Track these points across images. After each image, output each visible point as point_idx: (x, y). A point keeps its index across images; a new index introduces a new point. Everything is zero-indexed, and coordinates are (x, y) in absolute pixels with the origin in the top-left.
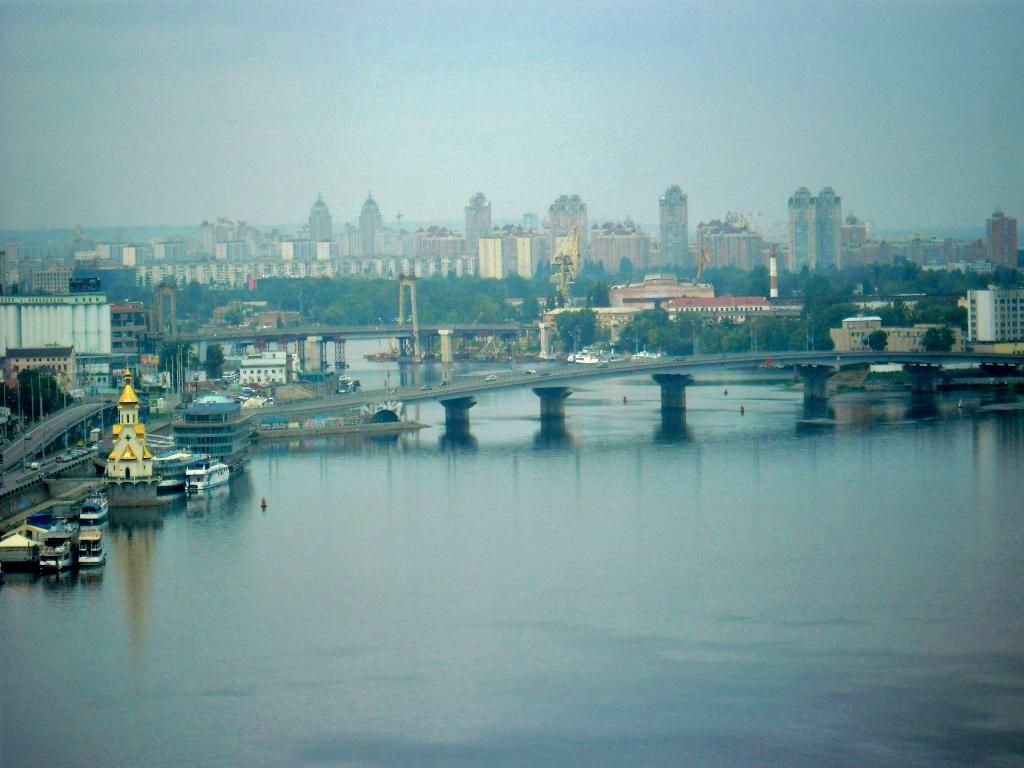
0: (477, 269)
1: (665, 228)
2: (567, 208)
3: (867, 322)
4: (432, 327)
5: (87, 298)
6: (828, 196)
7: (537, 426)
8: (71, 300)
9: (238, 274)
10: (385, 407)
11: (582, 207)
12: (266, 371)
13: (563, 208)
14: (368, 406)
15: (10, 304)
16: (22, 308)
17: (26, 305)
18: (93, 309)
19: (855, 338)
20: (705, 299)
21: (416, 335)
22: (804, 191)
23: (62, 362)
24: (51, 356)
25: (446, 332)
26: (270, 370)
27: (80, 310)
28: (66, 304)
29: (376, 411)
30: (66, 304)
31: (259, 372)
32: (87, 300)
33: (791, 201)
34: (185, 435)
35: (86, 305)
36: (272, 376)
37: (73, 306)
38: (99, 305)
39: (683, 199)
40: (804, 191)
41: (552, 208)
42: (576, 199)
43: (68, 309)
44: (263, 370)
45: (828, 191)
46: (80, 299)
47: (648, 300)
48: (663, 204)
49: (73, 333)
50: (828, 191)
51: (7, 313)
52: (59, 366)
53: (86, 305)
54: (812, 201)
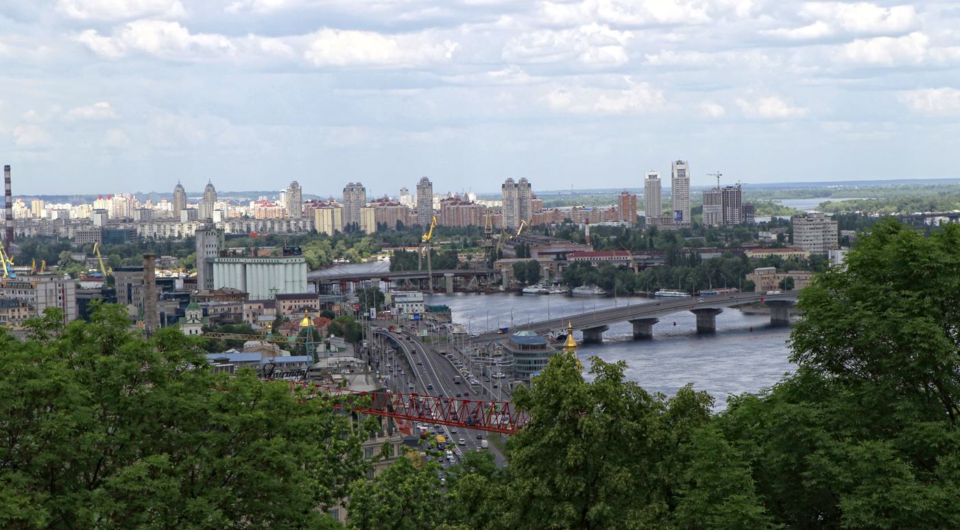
0: (313, 226)
1: (420, 202)
2: (354, 190)
3: (769, 270)
4: (440, 272)
5: (294, 259)
6: (524, 183)
7: (275, 318)
8: (284, 261)
9: (172, 230)
10: (562, 334)
11: (363, 189)
12: (412, 305)
13: (352, 190)
14: (553, 332)
15: (237, 263)
16: (248, 266)
17: (251, 264)
18: (297, 266)
19: (764, 281)
20: (588, 253)
21: (431, 277)
22: (510, 180)
24: (297, 299)
25: (450, 275)
26: (414, 304)
27: (290, 266)
28: (281, 263)
29: (557, 336)
30: (281, 263)
31: (408, 306)
32: (294, 261)
33: (503, 186)
34: (519, 358)
35: (293, 264)
36: (416, 308)
37: (286, 264)
38: (300, 264)
39: (430, 185)
40: (510, 180)
41: (344, 190)
42: (359, 185)
43: (282, 267)
44: (410, 304)
45: (523, 180)
46: (290, 260)
47: (553, 253)
48: (419, 187)
49: (286, 282)
50: (523, 180)
51: (251, 267)
53: (293, 264)
54: (516, 185)
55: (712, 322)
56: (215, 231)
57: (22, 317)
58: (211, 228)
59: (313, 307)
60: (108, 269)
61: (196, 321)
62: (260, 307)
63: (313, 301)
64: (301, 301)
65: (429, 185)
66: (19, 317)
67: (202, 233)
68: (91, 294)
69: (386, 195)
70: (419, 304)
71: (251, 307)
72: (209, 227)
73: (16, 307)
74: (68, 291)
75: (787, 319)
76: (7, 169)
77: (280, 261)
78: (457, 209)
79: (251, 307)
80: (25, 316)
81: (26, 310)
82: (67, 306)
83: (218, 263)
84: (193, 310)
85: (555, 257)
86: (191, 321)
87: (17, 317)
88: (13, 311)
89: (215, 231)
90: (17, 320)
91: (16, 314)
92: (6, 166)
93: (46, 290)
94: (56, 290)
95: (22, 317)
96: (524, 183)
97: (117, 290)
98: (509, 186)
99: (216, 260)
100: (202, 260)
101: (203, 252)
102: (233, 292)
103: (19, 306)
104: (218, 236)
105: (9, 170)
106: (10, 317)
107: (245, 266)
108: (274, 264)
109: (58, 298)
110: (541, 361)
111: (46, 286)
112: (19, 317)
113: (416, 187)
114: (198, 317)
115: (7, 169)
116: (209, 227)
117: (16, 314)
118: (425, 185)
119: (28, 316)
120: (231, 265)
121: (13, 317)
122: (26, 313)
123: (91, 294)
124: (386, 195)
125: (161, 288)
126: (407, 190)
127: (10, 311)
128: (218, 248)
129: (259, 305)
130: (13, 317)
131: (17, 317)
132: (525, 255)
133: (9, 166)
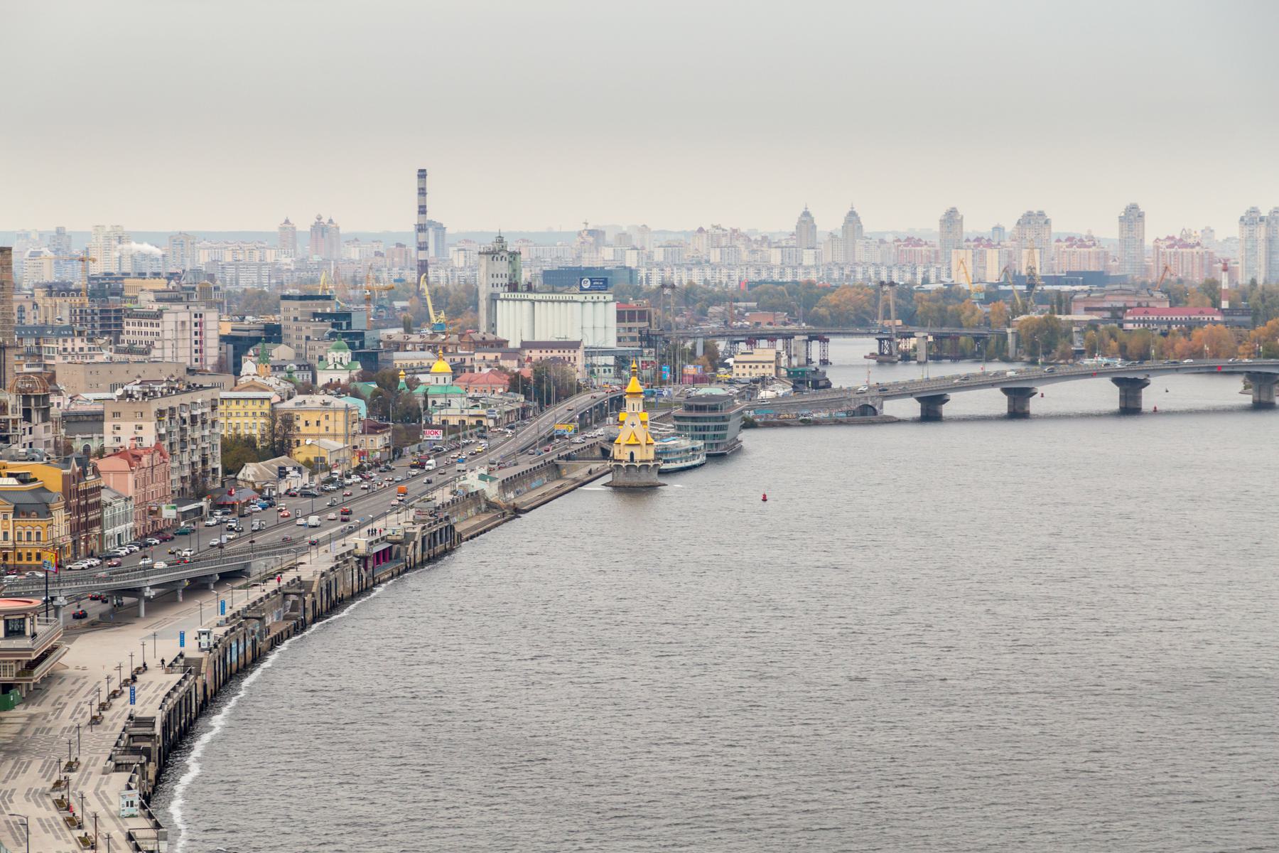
2: (1032, 223)
5: (595, 296)
15: (525, 300)
16: (536, 303)
17: (540, 301)
18: (601, 306)
22: (1254, 211)
23: (572, 354)
27: (601, 306)
28: (576, 302)
30: (576, 302)
35: (594, 303)
39: (1141, 216)
40: (1254, 211)
42: (1041, 214)
43: (526, 305)
52: (569, 358)
55: (1137, 398)
56: (505, 255)
57: (77, 349)
58: (500, 251)
59: (567, 359)
60: (439, 314)
61: (339, 367)
62: (496, 357)
63: (567, 351)
64: (554, 351)
65: (1139, 216)
66: (73, 349)
67: (485, 256)
68: (249, 331)
69: (1089, 231)
70: (767, 365)
71: (484, 357)
72: (497, 249)
73: (68, 335)
74: (208, 324)
75: (1271, 401)
76: (422, 174)
77: (576, 297)
78: (1176, 253)
79: (484, 357)
80: (81, 349)
81: (83, 341)
82: (206, 345)
83: (502, 300)
84: (337, 352)
85: (1107, 315)
86: (332, 367)
87: (69, 350)
88: (65, 341)
89: (505, 255)
90: (70, 354)
91: (69, 345)
92: (420, 171)
93: (176, 322)
94: (191, 321)
95: (77, 349)
96: (1253, 215)
97: (283, 326)
98: (1252, 219)
99: (502, 296)
100: (485, 296)
101: (487, 284)
102: (484, 339)
103: (73, 335)
104: (510, 262)
105: (424, 176)
106: (61, 348)
107: (534, 304)
108: (566, 302)
109: (193, 334)
110: (709, 426)
111: (177, 317)
112: (73, 349)
113: (1118, 219)
114: (343, 362)
115: (422, 174)
116: (497, 249)
117: (69, 345)
118: (1133, 217)
119: (86, 349)
120: (543, 303)
121: (65, 350)
122: (82, 345)
123: (249, 331)
124: (1089, 231)
125: (330, 323)
126: (1212, 231)
127: (61, 340)
128: (510, 280)
129: (496, 354)
130: (65, 350)
131: (69, 350)
132: (1064, 311)
133: (425, 170)
